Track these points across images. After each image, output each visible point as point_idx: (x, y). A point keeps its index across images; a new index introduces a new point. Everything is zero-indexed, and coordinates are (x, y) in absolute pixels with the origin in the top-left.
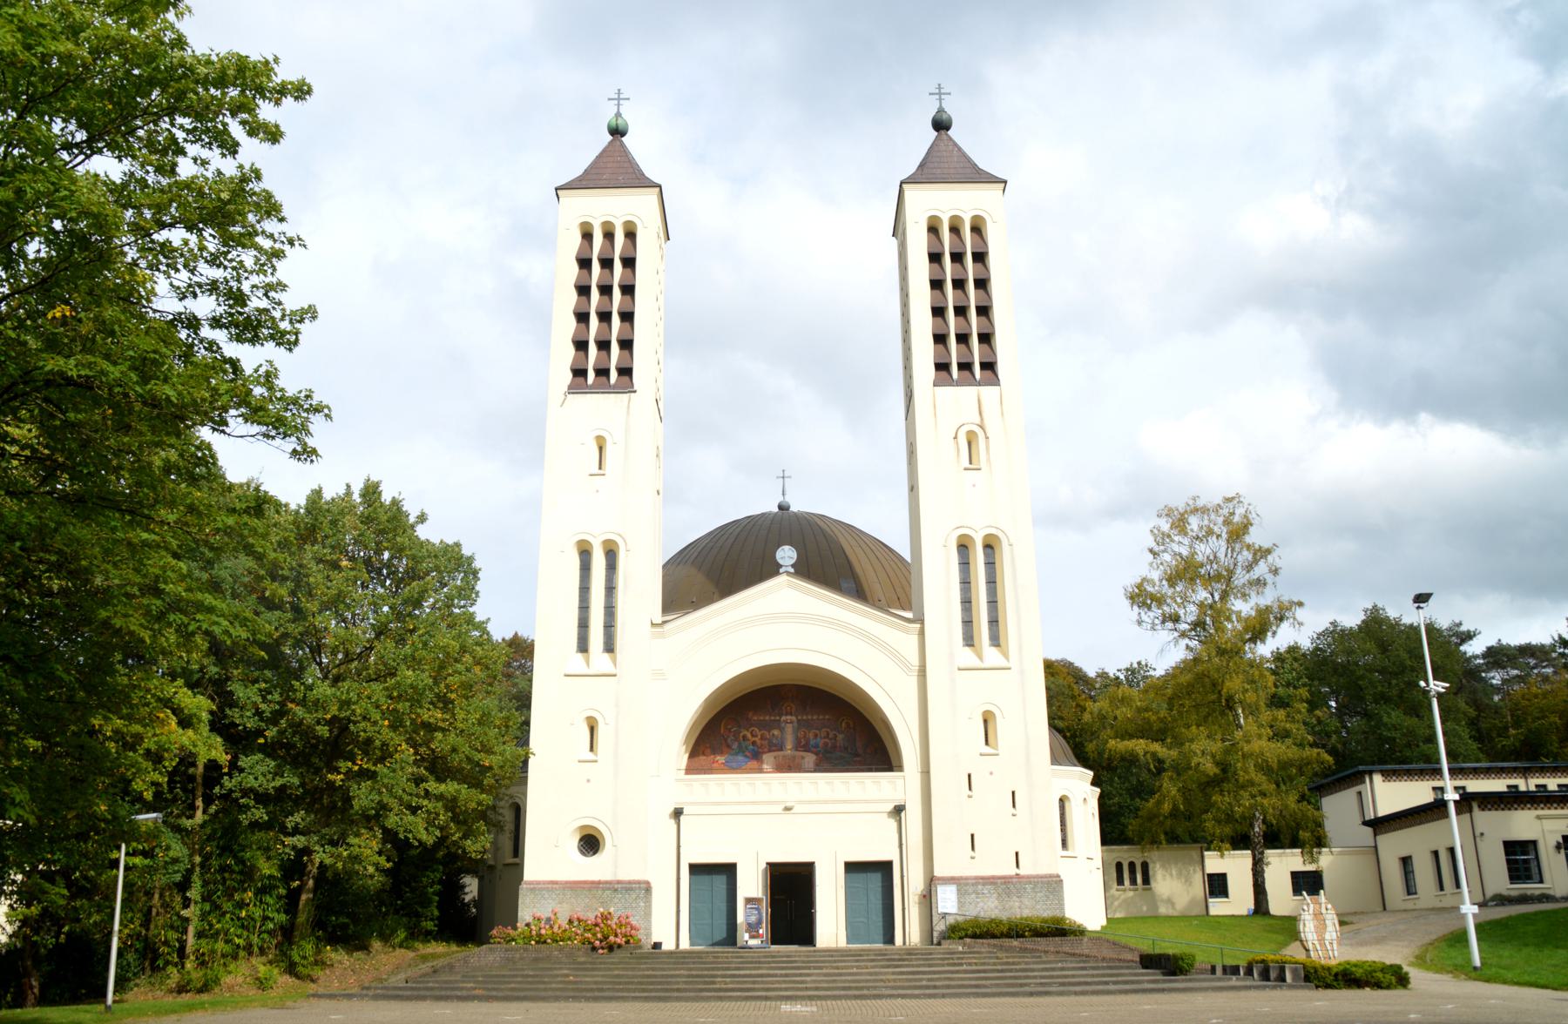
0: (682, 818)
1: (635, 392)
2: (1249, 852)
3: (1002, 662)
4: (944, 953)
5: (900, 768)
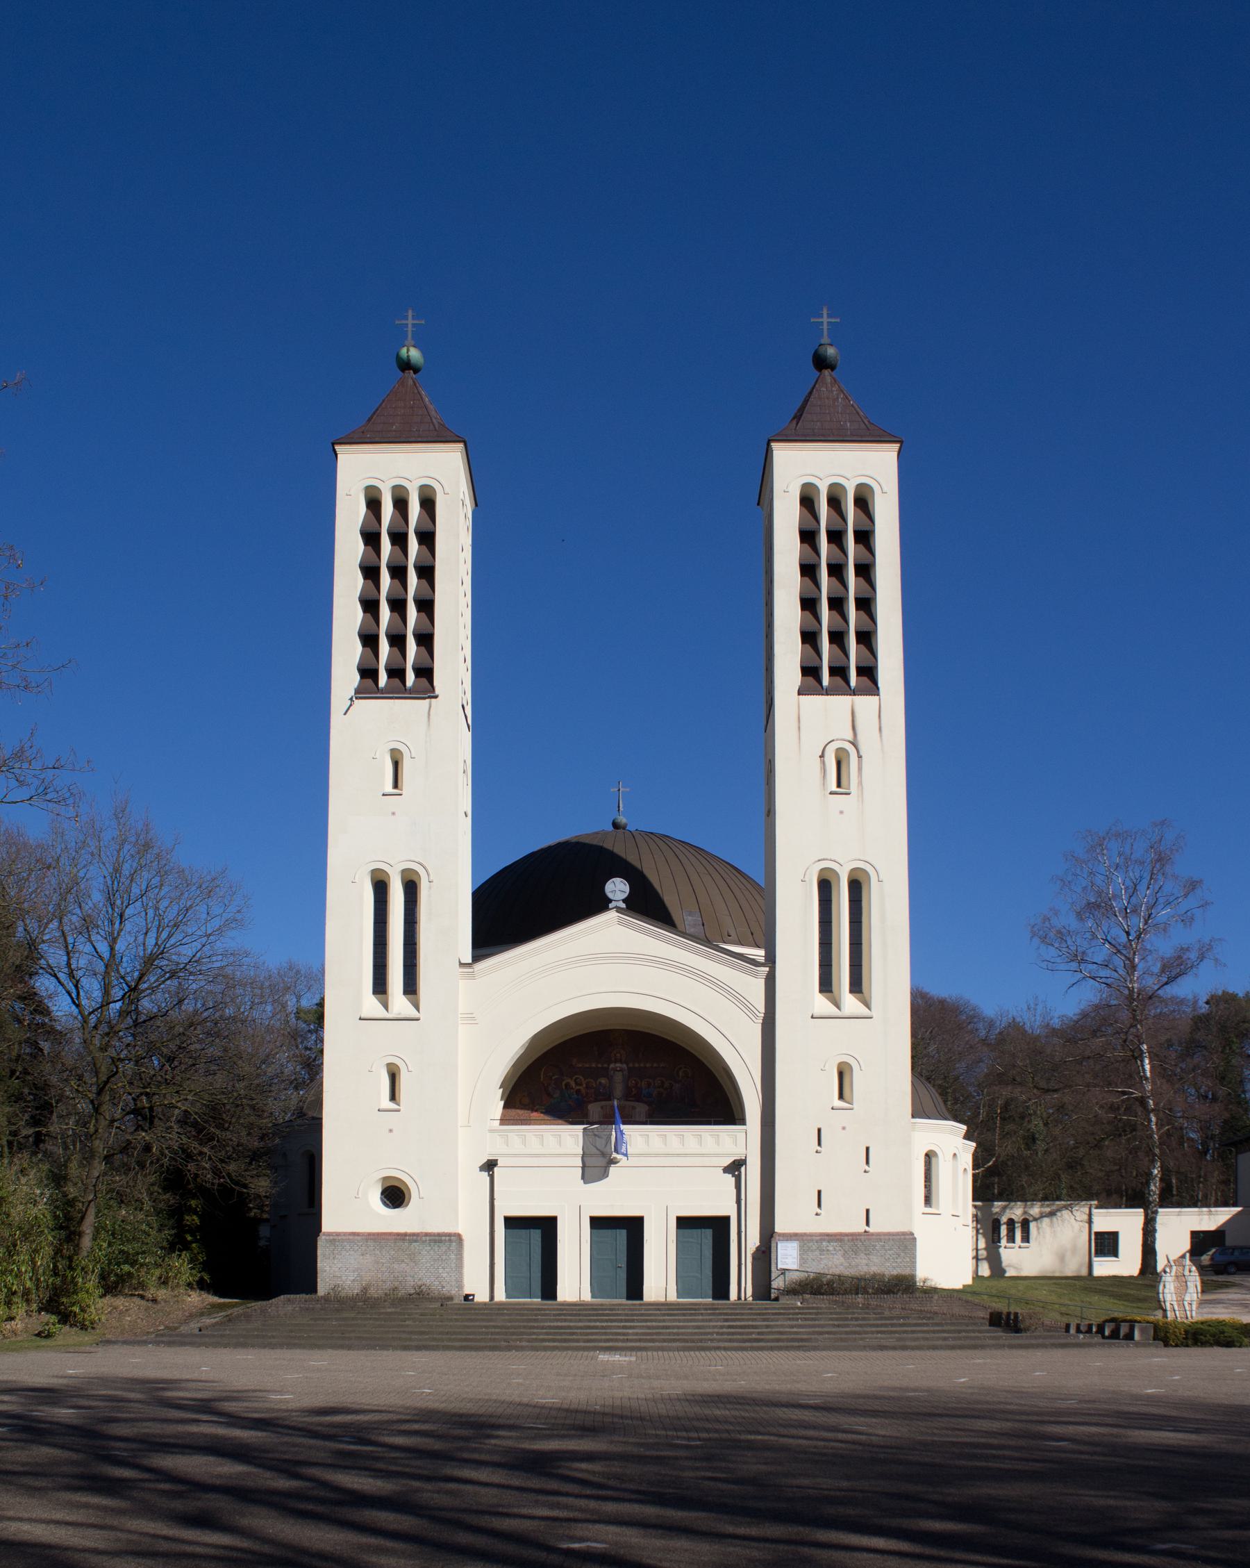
0: (496, 1169)
1: (436, 697)
2: (1142, 1210)
3: (862, 1010)
4: (782, 1308)
5: (742, 1121)
